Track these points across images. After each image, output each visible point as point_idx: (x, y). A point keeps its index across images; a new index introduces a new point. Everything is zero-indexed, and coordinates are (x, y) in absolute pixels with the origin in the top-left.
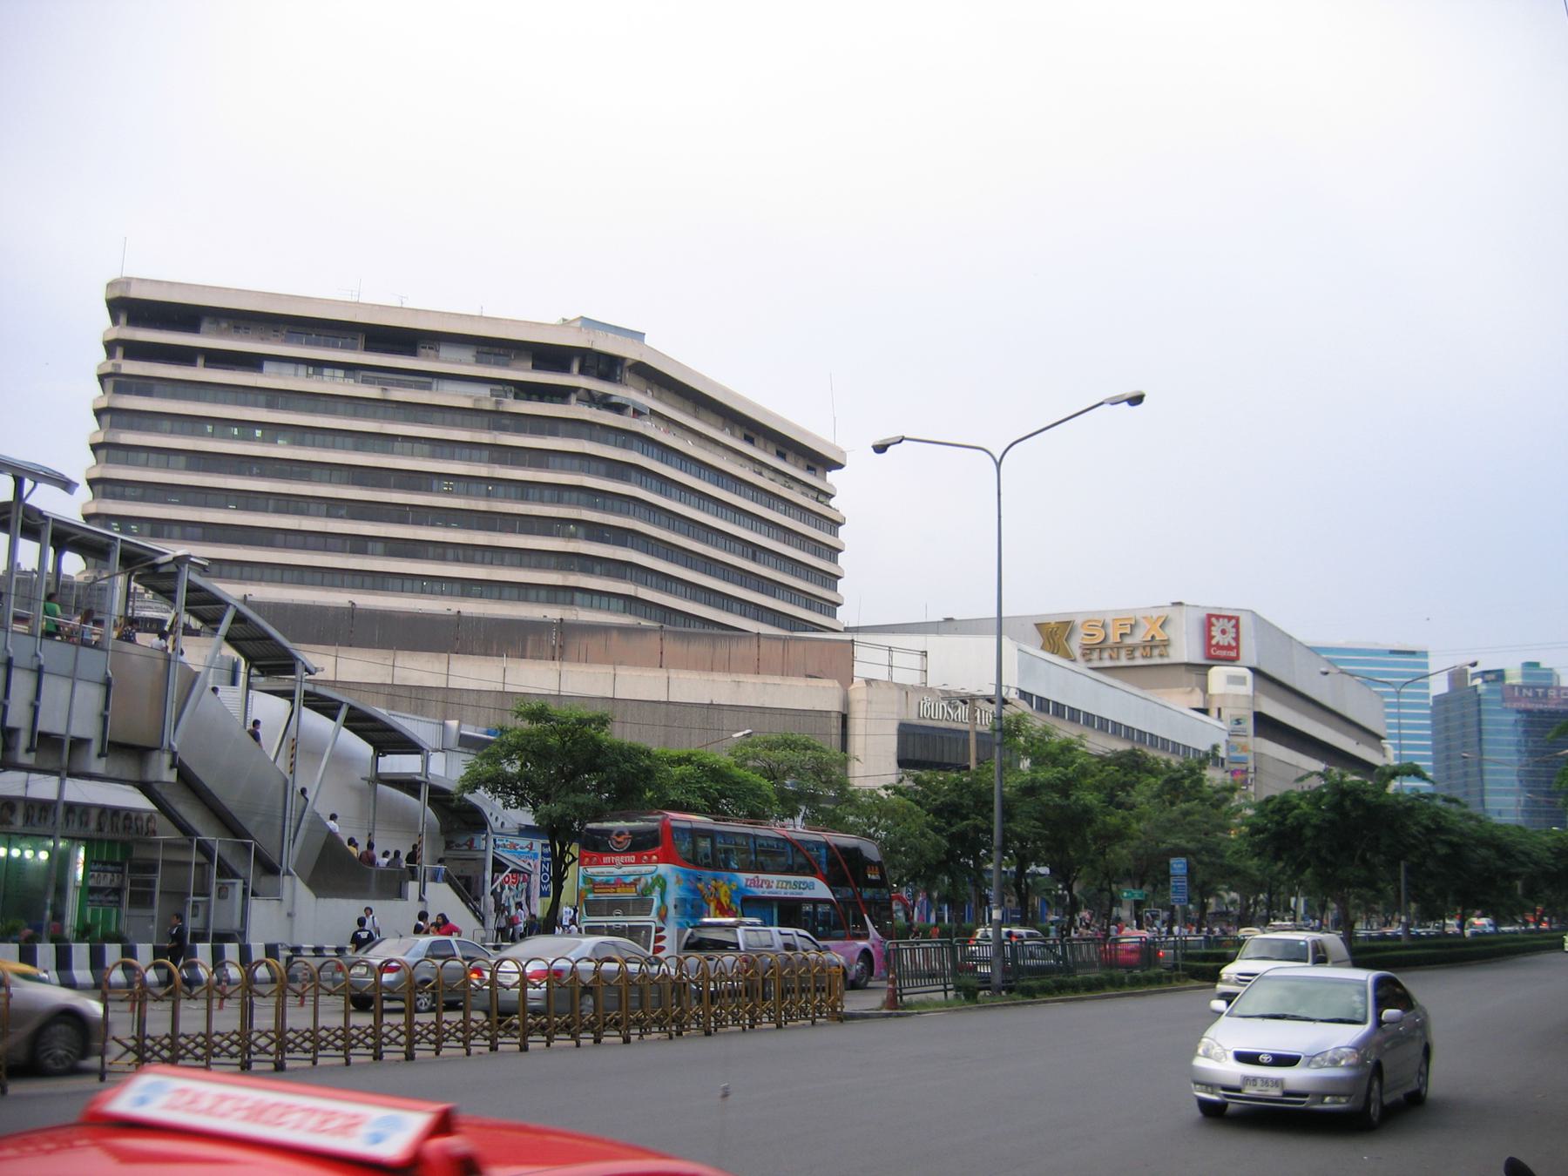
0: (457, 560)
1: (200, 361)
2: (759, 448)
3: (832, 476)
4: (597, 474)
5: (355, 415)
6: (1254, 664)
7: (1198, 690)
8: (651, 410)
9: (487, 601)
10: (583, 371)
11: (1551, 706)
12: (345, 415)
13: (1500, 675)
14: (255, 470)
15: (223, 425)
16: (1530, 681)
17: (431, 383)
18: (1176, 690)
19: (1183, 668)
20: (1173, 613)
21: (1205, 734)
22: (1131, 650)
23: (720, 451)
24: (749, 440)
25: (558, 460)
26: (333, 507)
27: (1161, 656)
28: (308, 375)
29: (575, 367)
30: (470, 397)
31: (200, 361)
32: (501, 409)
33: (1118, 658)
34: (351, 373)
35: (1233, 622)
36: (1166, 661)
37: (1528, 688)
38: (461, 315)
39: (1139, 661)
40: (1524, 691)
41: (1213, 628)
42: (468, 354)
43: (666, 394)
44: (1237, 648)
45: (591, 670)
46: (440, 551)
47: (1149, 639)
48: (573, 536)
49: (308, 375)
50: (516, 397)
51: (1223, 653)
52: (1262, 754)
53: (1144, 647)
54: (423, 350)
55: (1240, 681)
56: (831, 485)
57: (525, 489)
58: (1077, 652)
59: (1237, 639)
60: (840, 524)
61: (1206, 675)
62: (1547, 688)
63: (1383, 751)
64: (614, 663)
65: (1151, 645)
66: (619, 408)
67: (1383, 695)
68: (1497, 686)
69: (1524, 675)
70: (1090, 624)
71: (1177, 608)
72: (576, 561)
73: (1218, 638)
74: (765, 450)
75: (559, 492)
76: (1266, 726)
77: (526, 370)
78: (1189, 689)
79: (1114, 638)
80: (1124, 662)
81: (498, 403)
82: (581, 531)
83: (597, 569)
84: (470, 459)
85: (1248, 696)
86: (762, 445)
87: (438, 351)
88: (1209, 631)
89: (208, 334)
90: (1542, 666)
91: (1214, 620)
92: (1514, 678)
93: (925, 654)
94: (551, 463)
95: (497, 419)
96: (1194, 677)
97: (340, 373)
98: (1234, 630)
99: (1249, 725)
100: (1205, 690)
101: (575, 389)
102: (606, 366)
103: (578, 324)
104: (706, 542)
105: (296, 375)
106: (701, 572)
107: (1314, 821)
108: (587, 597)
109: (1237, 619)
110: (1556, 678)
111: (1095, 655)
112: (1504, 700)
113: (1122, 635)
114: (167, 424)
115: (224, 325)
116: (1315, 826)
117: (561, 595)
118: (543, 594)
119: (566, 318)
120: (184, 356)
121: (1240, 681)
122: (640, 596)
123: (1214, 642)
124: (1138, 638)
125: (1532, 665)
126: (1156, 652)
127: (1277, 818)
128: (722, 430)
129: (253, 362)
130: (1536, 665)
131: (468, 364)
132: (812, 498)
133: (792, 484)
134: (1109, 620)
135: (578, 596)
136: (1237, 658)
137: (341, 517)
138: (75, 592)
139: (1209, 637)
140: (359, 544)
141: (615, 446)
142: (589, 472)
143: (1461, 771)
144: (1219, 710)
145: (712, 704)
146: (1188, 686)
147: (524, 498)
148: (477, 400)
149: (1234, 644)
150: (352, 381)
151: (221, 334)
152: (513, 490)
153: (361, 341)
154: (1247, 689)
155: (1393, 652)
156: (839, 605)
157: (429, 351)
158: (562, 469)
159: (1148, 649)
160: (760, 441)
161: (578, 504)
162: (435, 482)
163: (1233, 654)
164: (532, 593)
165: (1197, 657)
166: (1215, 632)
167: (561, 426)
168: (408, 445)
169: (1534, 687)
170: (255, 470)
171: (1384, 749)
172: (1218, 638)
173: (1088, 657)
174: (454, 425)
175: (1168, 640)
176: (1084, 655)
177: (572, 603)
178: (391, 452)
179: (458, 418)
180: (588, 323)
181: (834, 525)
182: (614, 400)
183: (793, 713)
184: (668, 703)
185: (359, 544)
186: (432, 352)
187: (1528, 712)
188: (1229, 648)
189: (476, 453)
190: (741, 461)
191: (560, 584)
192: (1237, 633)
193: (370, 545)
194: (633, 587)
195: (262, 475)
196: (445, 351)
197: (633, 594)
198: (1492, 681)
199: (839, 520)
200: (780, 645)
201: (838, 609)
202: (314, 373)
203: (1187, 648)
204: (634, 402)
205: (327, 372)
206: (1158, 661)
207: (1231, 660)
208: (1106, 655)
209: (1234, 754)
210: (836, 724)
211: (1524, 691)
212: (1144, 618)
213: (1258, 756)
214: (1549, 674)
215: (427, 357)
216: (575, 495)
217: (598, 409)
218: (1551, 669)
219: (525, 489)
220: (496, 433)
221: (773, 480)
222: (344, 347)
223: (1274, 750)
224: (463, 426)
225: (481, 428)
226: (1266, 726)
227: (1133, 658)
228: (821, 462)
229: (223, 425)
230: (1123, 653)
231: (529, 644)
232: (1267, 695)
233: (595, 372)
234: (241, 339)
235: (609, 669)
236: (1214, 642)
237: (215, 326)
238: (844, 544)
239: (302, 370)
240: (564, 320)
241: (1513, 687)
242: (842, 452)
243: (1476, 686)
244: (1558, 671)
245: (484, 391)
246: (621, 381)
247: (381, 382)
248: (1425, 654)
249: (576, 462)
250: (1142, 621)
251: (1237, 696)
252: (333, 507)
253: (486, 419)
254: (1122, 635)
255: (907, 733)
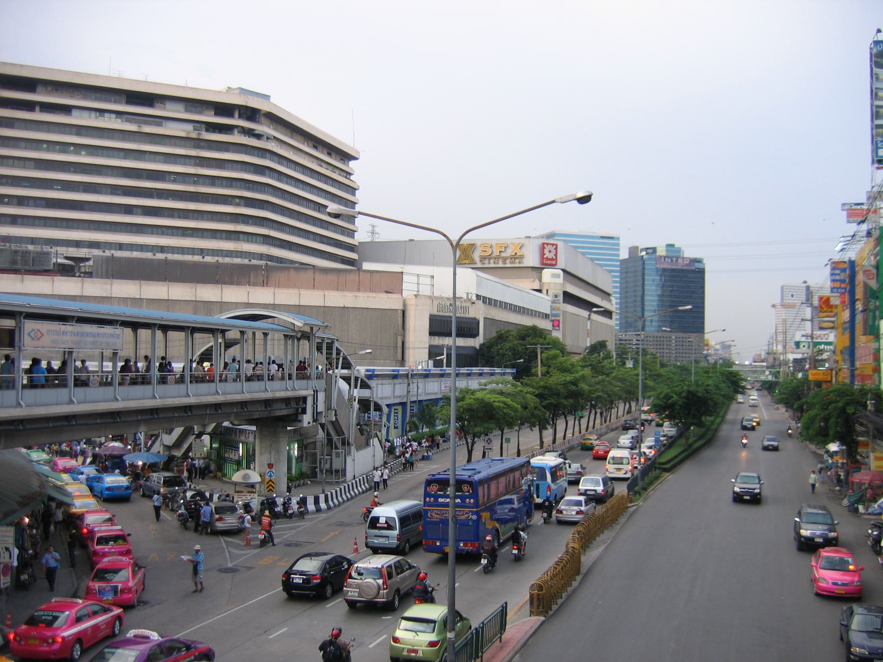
0: (180, 217)
1: (37, 109)
2: (320, 152)
3: (352, 163)
4: (249, 172)
5: (124, 140)
6: (563, 267)
7: (537, 281)
8: (274, 136)
9: (196, 239)
10: (240, 117)
11: (679, 267)
12: (119, 139)
13: (654, 250)
14: (72, 169)
15: (52, 145)
16: (669, 254)
17: (162, 122)
18: (526, 280)
19: (530, 269)
20: (526, 241)
21: (543, 303)
22: (505, 259)
23: (303, 155)
24: (315, 147)
25: (230, 165)
26: (115, 190)
27: (520, 263)
28: (96, 117)
29: (237, 115)
30: (184, 131)
31: (37, 109)
32: (201, 138)
33: (498, 263)
34: (119, 116)
35: (555, 247)
36: (522, 265)
37: (668, 257)
38: (179, 86)
39: (509, 265)
40: (667, 259)
41: (545, 250)
42: (180, 107)
43: (279, 127)
44: (556, 259)
45: (289, 292)
46: (171, 212)
47: (514, 254)
48: (238, 205)
49: (96, 117)
50: (207, 130)
51: (549, 262)
52: (566, 312)
53: (511, 258)
54: (157, 104)
55: (557, 276)
56: (352, 169)
57: (213, 181)
58: (477, 259)
59: (556, 255)
60: (356, 189)
61: (541, 273)
62: (678, 258)
63: (610, 301)
64: (298, 288)
65: (514, 257)
66: (258, 136)
67: (610, 271)
68: (653, 256)
69: (667, 251)
70: (484, 245)
71: (528, 239)
72: (240, 218)
73: (547, 255)
74: (322, 153)
75: (231, 182)
76: (568, 297)
77: (211, 116)
78: (532, 280)
79: (496, 253)
80: (501, 265)
81: (199, 134)
82: (242, 202)
83: (250, 221)
84: (185, 164)
85: (561, 284)
86: (321, 150)
87: (165, 105)
88: (543, 251)
89: (40, 93)
90: (676, 246)
91: (545, 246)
92: (661, 252)
93: (433, 277)
94: (226, 166)
95: (198, 143)
96: (535, 274)
97: (113, 116)
98: (555, 251)
99: (561, 298)
100: (540, 280)
101: (237, 127)
102: (251, 114)
103: (238, 91)
104: (298, 204)
105: (90, 117)
106: (296, 220)
107: (680, 403)
108: (246, 236)
109: (557, 245)
110: (682, 252)
111: (487, 261)
112: (656, 264)
113: (500, 252)
114: (23, 144)
115: (50, 88)
116: (679, 405)
117: (233, 236)
118: (224, 235)
119: (230, 87)
120: (29, 106)
121: (557, 276)
122: (271, 235)
123: (545, 257)
124: (508, 253)
125: (670, 246)
126: (517, 261)
127: (665, 401)
128: (304, 144)
129: (66, 109)
130: (673, 245)
131: (182, 113)
132: (343, 176)
133: (336, 170)
134: (494, 243)
135: (241, 236)
136: (556, 264)
137: (119, 195)
138: (32, 255)
139: (543, 254)
140: (129, 210)
141: (258, 157)
142: (246, 171)
143: (633, 299)
144: (547, 290)
145: (344, 307)
146: (532, 278)
147: (213, 185)
148: (188, 133)
149: (554, 257)
150: (120, 120)
151: (48, 93)
152: (207, 180)
153: (124, 99)
154: (560, 280)
155: (602, 237)
156: (355, 231)
157: (161, 105)
158: (232, 169)
159: (513, 259)
160: (320, 148)
161: (240, 188)
162: (167, 177)
163: (554, 262)
164: (219, 235)
165: (538, 265)
166: (546, 251)
167: (231, 147)
168: (152, 156)
169: (671, 258)
170: (72, 169)
171: (611, 300)
172: (547, 255)
173: (483, 262)
174: (176, 146)
175: (523, 255)
176: (481, 261)
177: (238, 240)
178: (144, 160)
179: (178, 142)
180: (243, 91)
181: (353, 190)
182: (256, 132)
183: (114, 187)
184: (325, 307)
185: (129, 210)
186: (162, 105)
187: (664, 270)
188: (552, 259)
189: (188, 160)
190: (312, 159)
191: (233, 230)
192: (556, 252)
193: (135, 210)
194: (268, 230)
195: (75, 172)
196: (169, 105)
197: (268, 234)
198: (651, 253)
199: (356, 188)
200: (369, 274)
201: (355, 233)
202: (100, 116)
203: (532, 259)
204: (266, 133)
205: (106, 115)
206: (518, 265)
207: (553, 266)
208: (492, 261)
209: (553, 312)
210: (400, 314)
211: (667, 259)
212: (512, 244)
213: (565, 313)
214: (679, 250)
215: (160, 109)
216: (239, 183)
217: (249, 137)
218: (680, 248)
219: (213, 181)
220: (198, 150)
221: (327, 169)
222: (115, 102)
223: (571, 309)
224: (180, 146)
225: (190, 147)
226: (568, 297)
227: (505, 264)
228: (346, 157)
229: (52, 145)
230: (500, 261)
231: (252, 275)
232: (571, 283)
233: (245, 116)
234: (60, 97)
235: (296, 291)
236: (545, 257)
237: (44, 88)
238: (358, 200)
239: (93, 114)
240: (229, 88)
241: (661, 257)
242: (358, 152)
243: (642, 256)
244: (683, 249)
245: (189, 127)
246: (259, 121)
247: (136, 122)
248: (618, 239)
249: (239, 166)
250: (511, 245)
251: (555, 284)
252: (115, 190)
253: (192, 143)
254: (500, 252)
255: (433, 320)
